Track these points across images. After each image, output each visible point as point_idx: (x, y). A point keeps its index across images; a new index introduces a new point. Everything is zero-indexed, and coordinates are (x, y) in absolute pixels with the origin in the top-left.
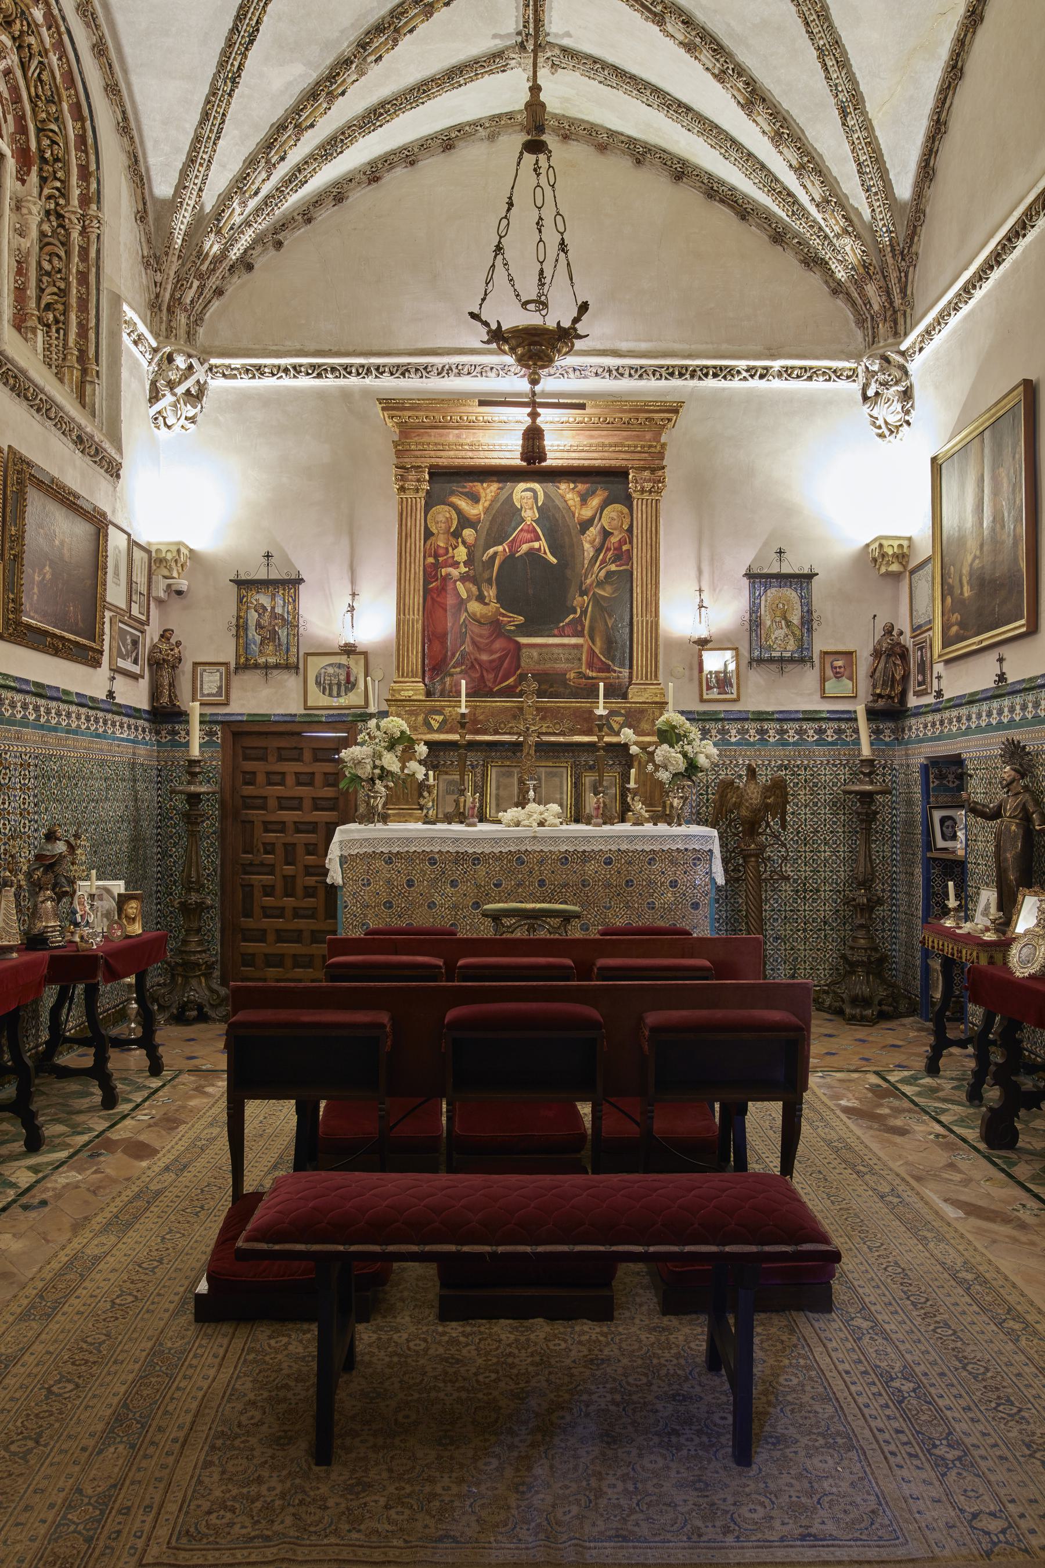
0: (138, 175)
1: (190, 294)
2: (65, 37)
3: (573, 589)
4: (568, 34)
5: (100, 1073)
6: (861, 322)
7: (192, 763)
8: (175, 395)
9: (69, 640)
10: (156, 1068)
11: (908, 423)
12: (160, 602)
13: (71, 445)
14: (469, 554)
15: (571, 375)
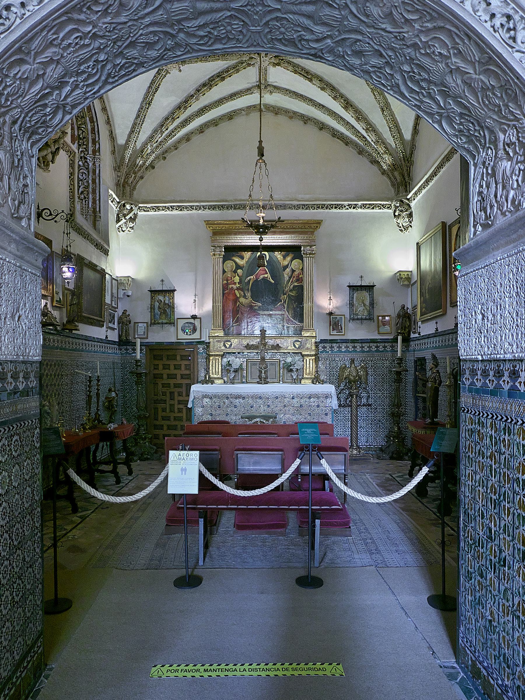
0: (112, 137)
4: (276, 82)
5: (114, 472)
7: (137, 361)
8: (126, 219)
10: (130, 473)
11: (411, 226)
14: (240, 280)
15: (279, 208)
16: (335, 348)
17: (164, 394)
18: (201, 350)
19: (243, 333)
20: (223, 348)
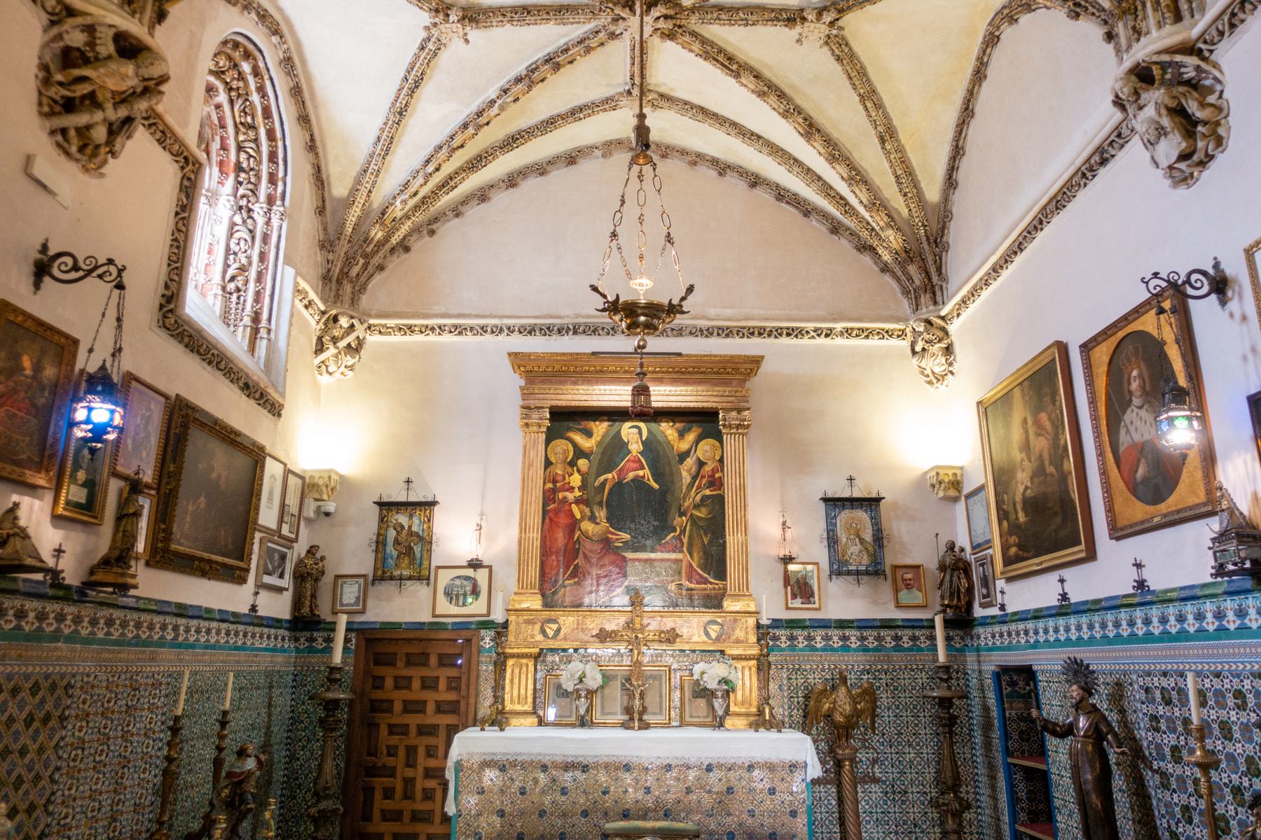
1: (355, 270)
2: (268, 83)
3: (674, 510)
6: (906, 293)
7: (333, 670)
9: (217, 563)
11: (952, 373)
12: (309, 521)
13: (239, 392)
14: (583, 481)
16: (801, 639)
17: (392, 751)
18: (487, 642)
19: (586, 601)
20: (540, 637)
